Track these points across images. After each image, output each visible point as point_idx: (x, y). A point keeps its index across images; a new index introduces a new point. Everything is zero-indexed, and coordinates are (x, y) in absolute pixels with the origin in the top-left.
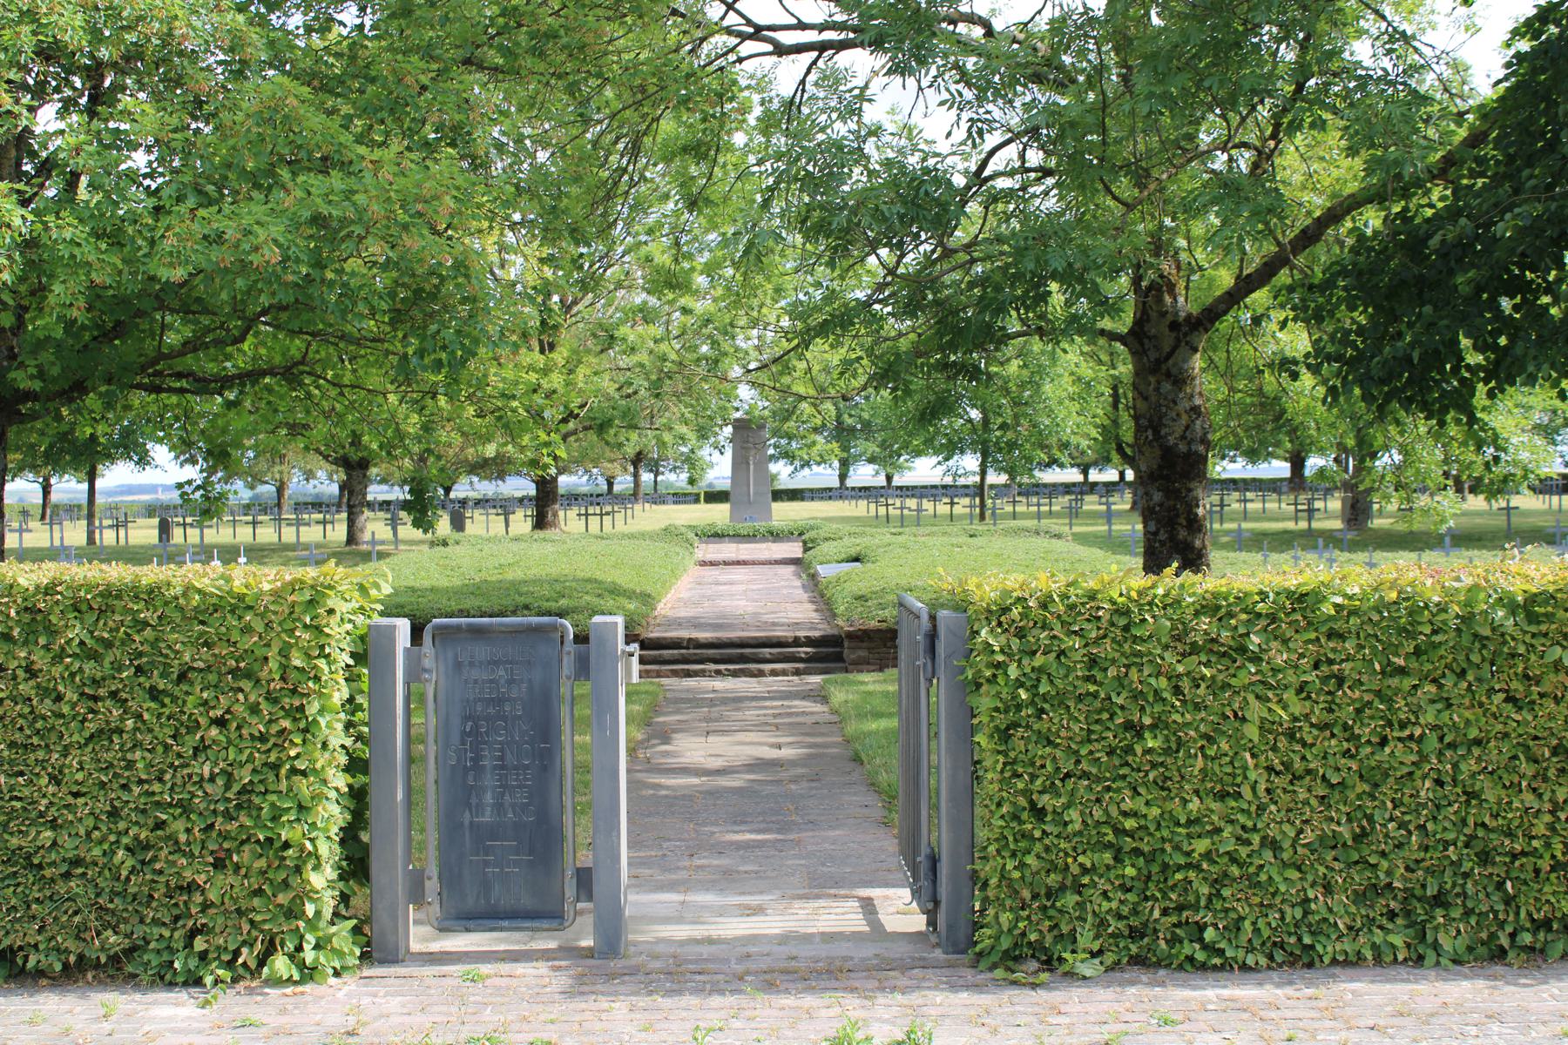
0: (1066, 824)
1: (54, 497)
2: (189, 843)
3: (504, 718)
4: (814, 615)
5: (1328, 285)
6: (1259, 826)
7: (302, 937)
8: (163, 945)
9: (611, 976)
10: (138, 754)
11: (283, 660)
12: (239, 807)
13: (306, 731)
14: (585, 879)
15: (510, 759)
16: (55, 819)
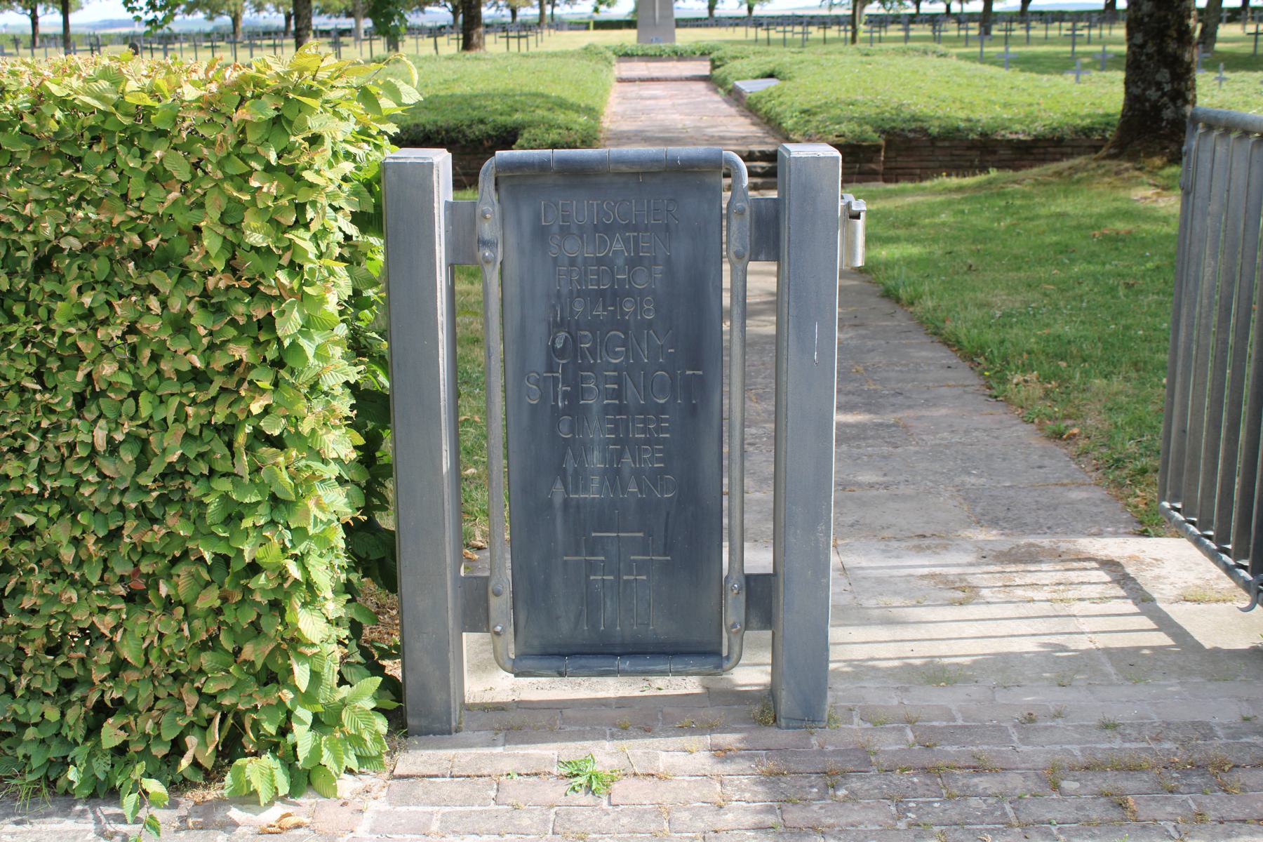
2: (79, 563)
3: (623, 326)
4: (754, 128)
7: (289, 714)
11: (230, 234)
12: (164, 500)
13: (279, 364)
15: (632, 393)
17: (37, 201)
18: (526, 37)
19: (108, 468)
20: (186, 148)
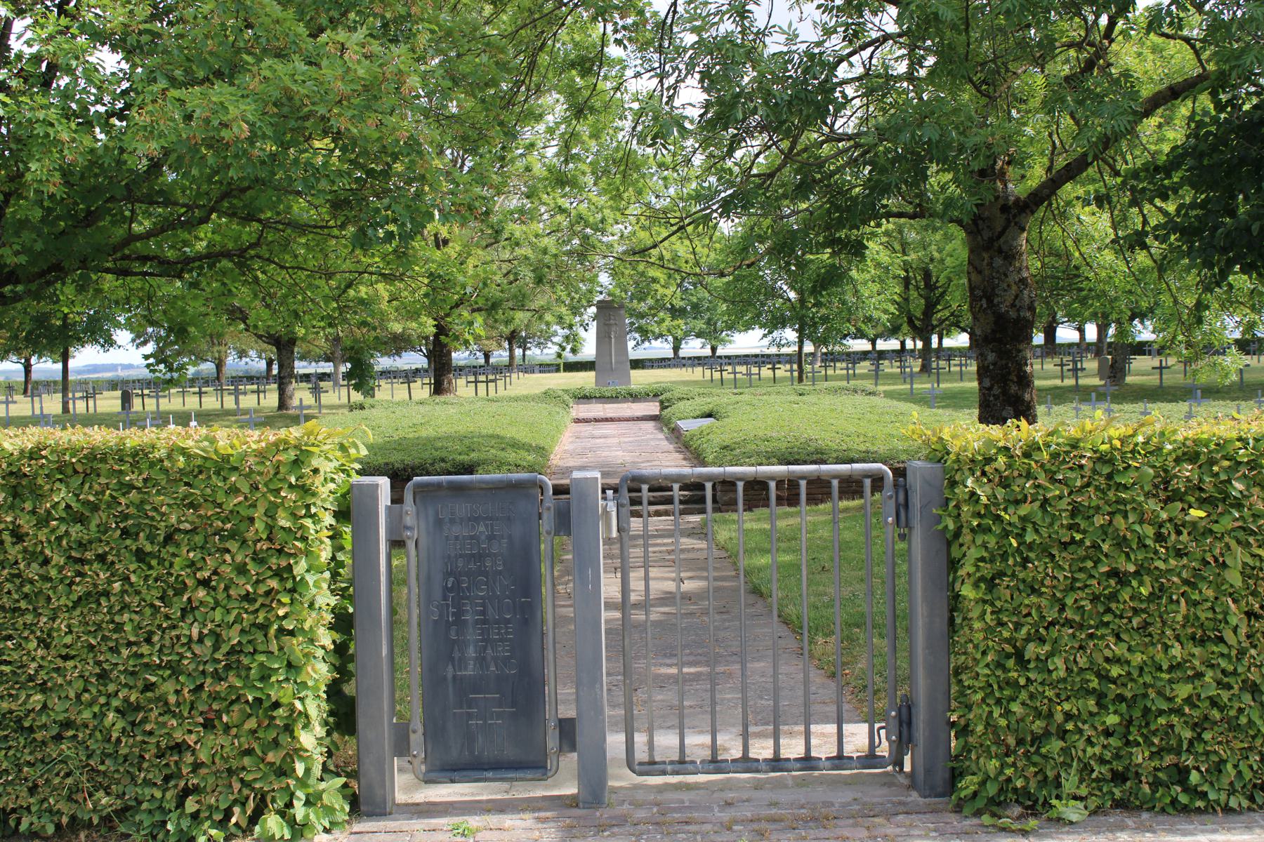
0: (1050, 672)
1: (34, 376)
2: (178, 704)
3: (486, 574)
5: (1168, 169)
6: (1240, 670)
7: (292, 795)
8: (156, 805)
9: (601, 828)
10: (126, 617)
11: (269, 521)
12: (228, 667)
14: (567, 730)
15: (492, 613)
16: (45, 683)
17: (168, 505)
18: (494, 381)
19: (197, 649)
20: (247, 476)
